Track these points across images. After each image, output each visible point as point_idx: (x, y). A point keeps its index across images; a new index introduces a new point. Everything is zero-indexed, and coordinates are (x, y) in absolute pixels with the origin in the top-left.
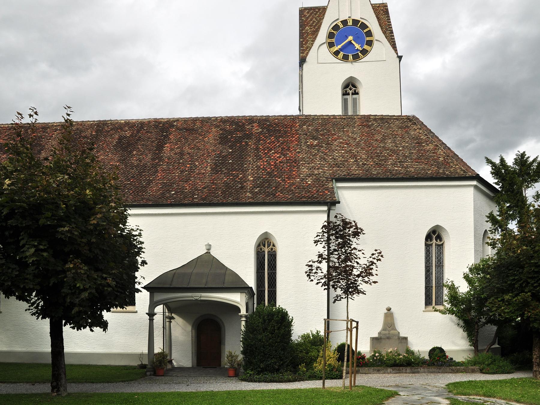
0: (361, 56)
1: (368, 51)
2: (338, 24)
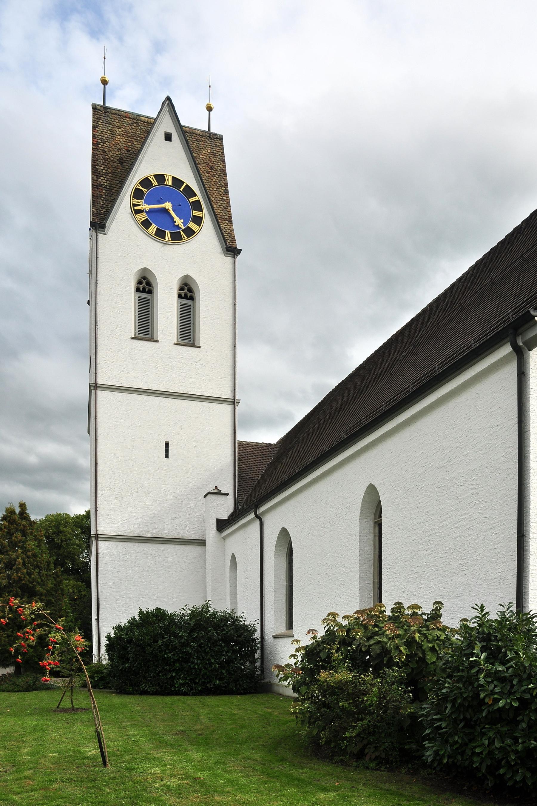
0: (184, 237)
2: (166, 176)
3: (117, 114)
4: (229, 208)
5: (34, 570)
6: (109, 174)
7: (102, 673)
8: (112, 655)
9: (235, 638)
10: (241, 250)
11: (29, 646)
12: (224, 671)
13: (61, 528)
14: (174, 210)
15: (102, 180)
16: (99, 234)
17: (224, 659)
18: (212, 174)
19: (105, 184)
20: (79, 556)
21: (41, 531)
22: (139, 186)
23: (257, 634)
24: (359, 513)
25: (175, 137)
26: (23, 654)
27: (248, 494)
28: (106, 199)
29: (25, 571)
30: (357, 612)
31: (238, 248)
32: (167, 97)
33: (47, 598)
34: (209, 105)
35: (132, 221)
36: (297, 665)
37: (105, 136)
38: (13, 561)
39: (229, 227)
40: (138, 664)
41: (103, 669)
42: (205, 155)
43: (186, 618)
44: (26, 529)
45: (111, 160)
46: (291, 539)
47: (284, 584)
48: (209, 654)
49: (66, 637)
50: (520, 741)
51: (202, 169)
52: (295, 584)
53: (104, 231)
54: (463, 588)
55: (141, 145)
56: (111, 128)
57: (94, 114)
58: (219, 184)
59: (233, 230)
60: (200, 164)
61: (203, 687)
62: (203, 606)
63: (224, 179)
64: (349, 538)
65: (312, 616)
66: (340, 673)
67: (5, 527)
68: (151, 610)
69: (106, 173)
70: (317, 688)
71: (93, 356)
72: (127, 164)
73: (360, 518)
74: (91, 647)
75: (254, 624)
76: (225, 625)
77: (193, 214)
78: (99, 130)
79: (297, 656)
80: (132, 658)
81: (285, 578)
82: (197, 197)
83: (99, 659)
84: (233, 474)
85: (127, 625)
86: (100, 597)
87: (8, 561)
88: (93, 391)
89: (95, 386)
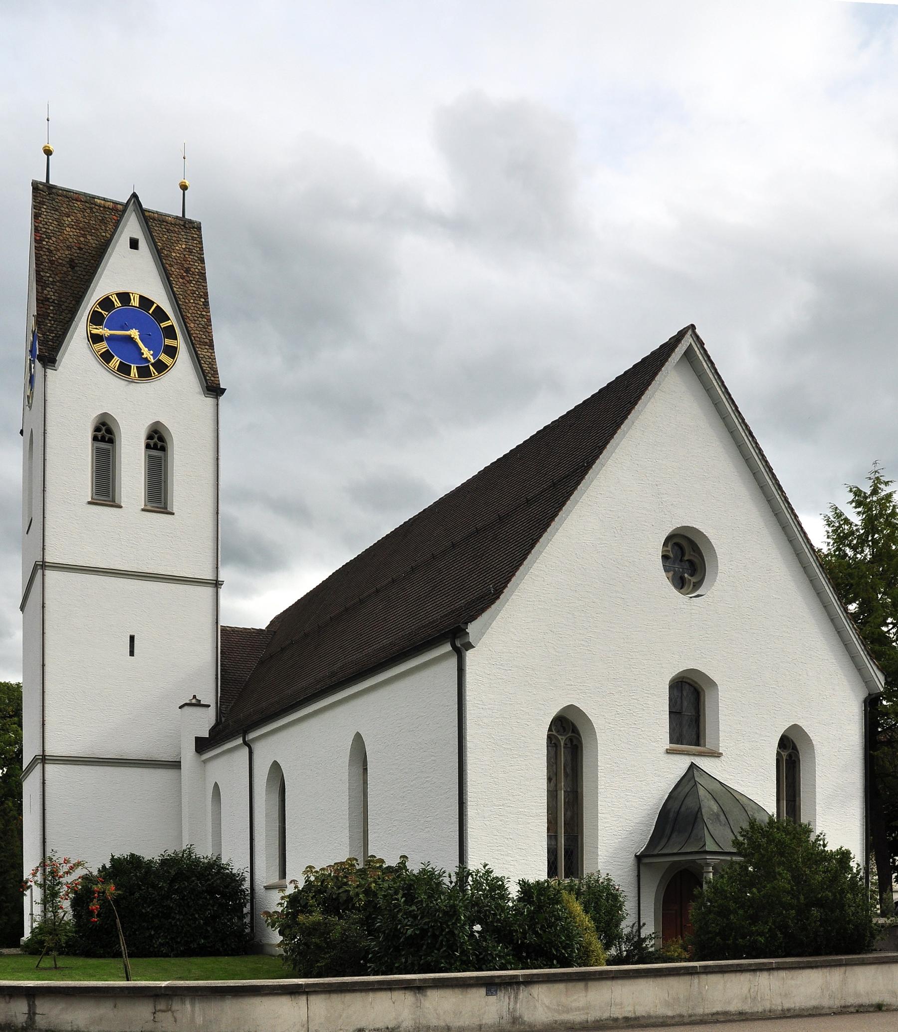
0: (154, 373)
1: (168, 367)
2: (131, 294)
3: (64, 196)
4: (209, 327)
6: (58, 284)
10: (226, 389)
12: (209, 929)
15: (49, 292)
16: (48, 370)
22: (98, 308)
23: (247, 885)
25: (143, 244)
28: (54, 319)
31: (221, 387)
32: (132, 194)
35: (89, 352)
37: (51, 228)
40: (111, 920)
42: (179, 252)
45: (58, 262)
46: (283, 775)
48: (193, 909)
50: (423, 958)
53: (55, 367)
54: (428, 843)
56: (58, 217)
57: (35, 197)
58: (197, 293)
59: (215, 359)
61: (186, 948)
63: (203, 286)
69: (54, 281)
72: (80, 269)
77: (166, 343)
78: (42, 219)
82: (170, 321)
84: (214, 677)
86: (47, 837)
89: (42, 565)
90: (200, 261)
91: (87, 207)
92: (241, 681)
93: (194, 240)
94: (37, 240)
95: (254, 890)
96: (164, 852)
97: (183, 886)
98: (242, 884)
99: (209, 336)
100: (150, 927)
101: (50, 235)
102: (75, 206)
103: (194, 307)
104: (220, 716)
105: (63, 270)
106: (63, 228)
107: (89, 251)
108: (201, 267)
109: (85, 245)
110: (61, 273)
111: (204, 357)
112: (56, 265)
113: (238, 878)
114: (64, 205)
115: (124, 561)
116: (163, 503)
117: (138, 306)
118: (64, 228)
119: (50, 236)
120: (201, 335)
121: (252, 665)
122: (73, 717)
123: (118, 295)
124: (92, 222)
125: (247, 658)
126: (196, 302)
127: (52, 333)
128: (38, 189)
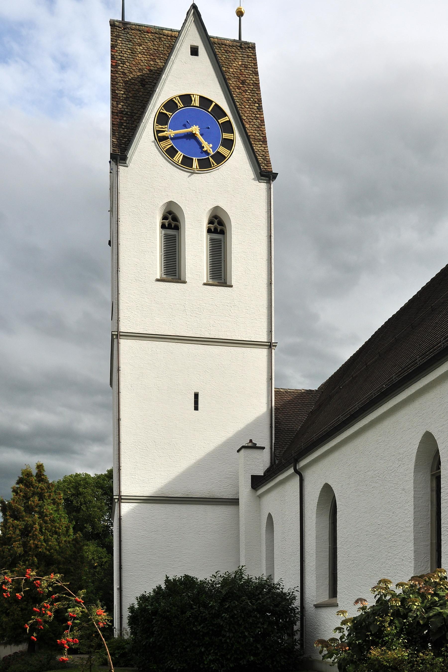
2: (192, 96)
3: (137, 30)
5: (52, 537)
6: (131, 99)
7: (124, 649)
8: (135, 628)
9: (272, 608)
11: (46, 622)
12: (259, 646)
13: (80, 489)
14: (202, 135)
16: (120, 167)
17: (259, 631)
18: (244, 89)
19: (126, 110)
20: (99, 520)
21: (60, 494)
22: (163, 110)
23: (297, 603)
24: (413, 465)
25: (202, 51)
26: (38, 631)
27: (286, 447)
29: (42, 538)
30: (413, 578)
31: (273, 172)
32: (192, 5)
33: (65, 567)
34: (240, 10)
35: (156, 149)
36: (343, 640)
37: (125, 55)
38: (29, 527)
39: (263, 148)
41: (124, 644)
43: (217, 586)
44: (43, 492)
45: (131, 82)
46: (334, 496)
47: (326, 546)
48: (243, 627)
49: (86, 611)
51: (232, 85)
52: (340, 546)
55: (165, 63)
58: (252, 100)
60: (230, 79)
62: (236, 572)
64: (402, 493)
65: (359, 582)
66: (394, 650)
67: (21, 491)
68: (179, 578)
69: (127, 97)
70: (366, 667)
71: (115, 302)
72: (150, 86)
73: (414, 471)
74: (112, 621)
75: (293, 592)
76: (261, 593)
77: (223, 137)
78: (118, 49)
79: (343, 629)
80: (157, 631)
81: (328, 540)
83: (121, 633)
85: (152, 594)
86: (123, 564)
87: (23, 527)
88: (115, 341)
89: (117, 335)
90: (254, 74)
91: (156, 37)
92: (293, 431)
93: (249, 58)
94: (113, 65)
95: (304, 608)
96: (216, 573)
97: (233, 605)
98: (291, 603)
99: (263, 134)
100: (200, 644)
101: (125, 61)
102: (146, 37)
103: (249, 111)
104: (274, 459)
105: (135, 88)
106: (135, 55)
107: (157, 71)
108: (255, 78)
109: (154, 67)
110: (133, 90)
111: (259, 151)
112: (129, 84)
113: (288, 597)
114: (137, 37)
115: (189, 329)
116: (223, 280)
117: (198, 106)
118: (137, 55)
119: (124, 62)
120: (256, 133)
121: (302, 418)
122: (145, 463)
123: (181, 97)
124: (160, 49)
125: (298, 412)
126: (251, 107)
127: (125, 138)
128: (114, 25)
